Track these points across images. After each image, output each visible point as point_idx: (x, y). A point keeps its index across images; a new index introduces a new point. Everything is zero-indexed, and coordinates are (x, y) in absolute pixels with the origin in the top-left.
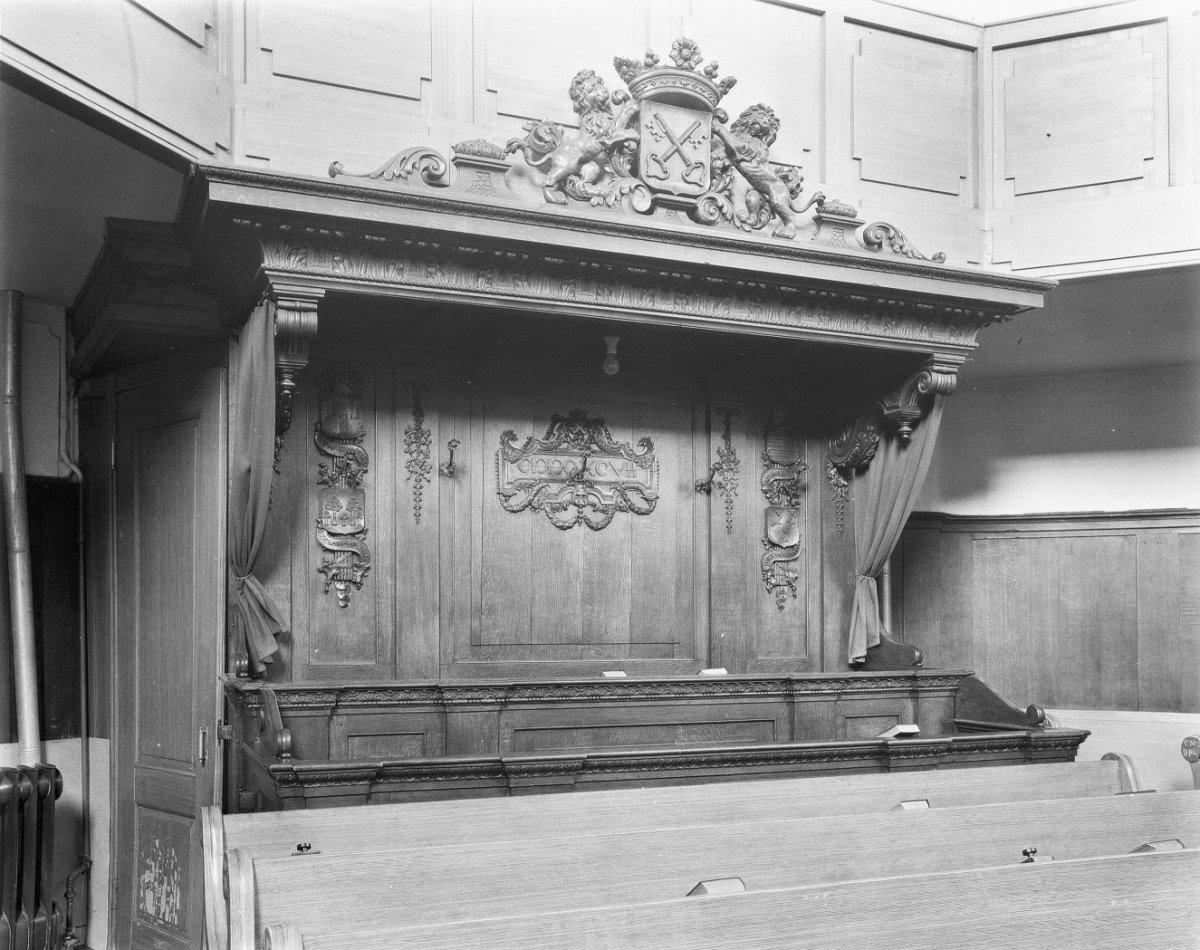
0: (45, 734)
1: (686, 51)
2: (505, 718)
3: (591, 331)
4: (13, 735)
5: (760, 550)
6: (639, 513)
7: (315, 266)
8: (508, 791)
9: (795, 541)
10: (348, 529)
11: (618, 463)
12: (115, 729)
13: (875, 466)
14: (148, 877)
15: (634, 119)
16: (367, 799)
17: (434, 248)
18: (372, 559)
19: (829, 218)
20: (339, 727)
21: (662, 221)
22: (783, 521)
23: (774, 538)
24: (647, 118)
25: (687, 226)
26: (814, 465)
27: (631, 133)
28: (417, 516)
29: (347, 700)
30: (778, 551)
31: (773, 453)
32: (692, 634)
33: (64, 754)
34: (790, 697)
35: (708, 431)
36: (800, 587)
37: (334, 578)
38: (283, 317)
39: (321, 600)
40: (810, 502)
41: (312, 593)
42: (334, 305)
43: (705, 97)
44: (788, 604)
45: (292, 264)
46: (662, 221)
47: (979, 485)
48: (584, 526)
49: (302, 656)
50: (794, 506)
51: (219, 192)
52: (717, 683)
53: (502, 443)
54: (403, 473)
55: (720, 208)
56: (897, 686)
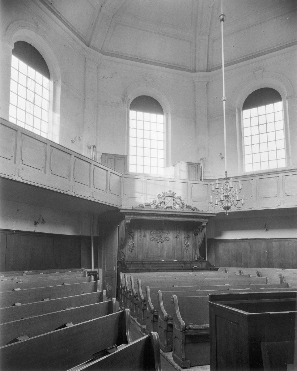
0: (95, 268)
1: (170, 191)
2: (150, 265)
3: (160, 222)
4: (91, 268)
5: (184, 245)
6: (167, 240)
8: (150, 272)
10: (132, 243)
11: (165, 234)
12: (103, 267)
13: (199, 234)
14: (107, 285)
16: (135, 272)
17: (132, 310)
18: (123, 104)
19: (189, 207)
20: (132, 266)
22: (187, 241)
23: (186, 244)
26: (191, 234)
27: (164, 200)
31: (185, 233)
32: (174, 256)
33: (96, 270)
34: (184, 264)
35: (176, 230)
38: (126, 222)
40: (191, 239)
42: (132, 220)
43: (173, 196)
44: (188, 252)
45: (128, 216)
47: (220, 234)
48: (160, 243)
49: (126, 258)
50: (188, 239)
51: (121, 211)
52: (175, 262)
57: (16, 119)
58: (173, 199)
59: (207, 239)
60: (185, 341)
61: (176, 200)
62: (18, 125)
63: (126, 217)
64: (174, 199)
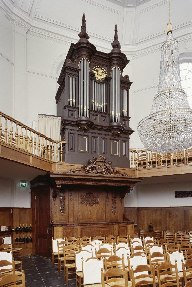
7: (60, 182)
9: (116, 207)
15: (95, 164)
21: (98, 175)
23: (113, 207)
24: (97, 163)
25: (101, 175)
27: (95, 165)
28: (71, 205)
29: (64, 225)
30: (114, 208)
36: (117, 212)
37: (62, 212)
39: (60, 215)
41: (59, 214)
44: (115, 214)
45: (58, 181)
46: (98, 175)
51: (51, 176)
53: (81, 196)
54: (69, 200)
55: (105, 172)
56: (126, 223)
57: (182, 70)
58: (104, 164)
59: (181, 161)
60: (151, 210)
61: (106, 165)
62: (114, 35)
63: (57, 182)
64: (105, 164)
